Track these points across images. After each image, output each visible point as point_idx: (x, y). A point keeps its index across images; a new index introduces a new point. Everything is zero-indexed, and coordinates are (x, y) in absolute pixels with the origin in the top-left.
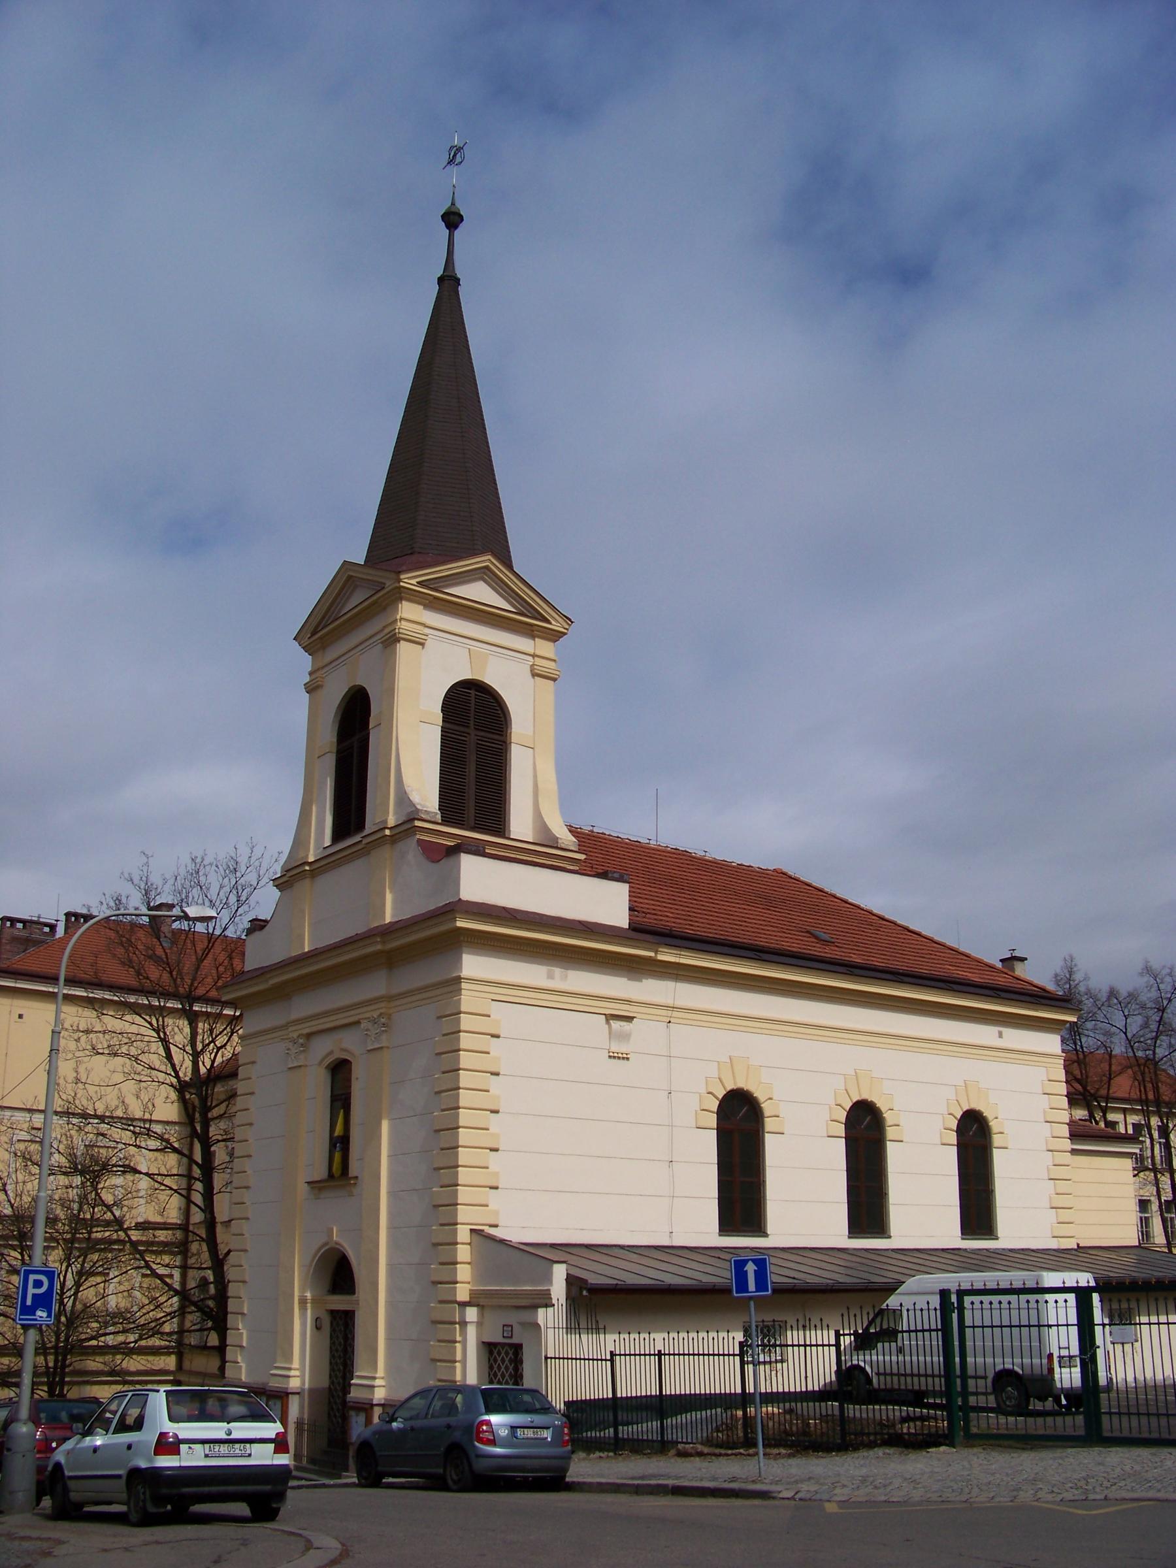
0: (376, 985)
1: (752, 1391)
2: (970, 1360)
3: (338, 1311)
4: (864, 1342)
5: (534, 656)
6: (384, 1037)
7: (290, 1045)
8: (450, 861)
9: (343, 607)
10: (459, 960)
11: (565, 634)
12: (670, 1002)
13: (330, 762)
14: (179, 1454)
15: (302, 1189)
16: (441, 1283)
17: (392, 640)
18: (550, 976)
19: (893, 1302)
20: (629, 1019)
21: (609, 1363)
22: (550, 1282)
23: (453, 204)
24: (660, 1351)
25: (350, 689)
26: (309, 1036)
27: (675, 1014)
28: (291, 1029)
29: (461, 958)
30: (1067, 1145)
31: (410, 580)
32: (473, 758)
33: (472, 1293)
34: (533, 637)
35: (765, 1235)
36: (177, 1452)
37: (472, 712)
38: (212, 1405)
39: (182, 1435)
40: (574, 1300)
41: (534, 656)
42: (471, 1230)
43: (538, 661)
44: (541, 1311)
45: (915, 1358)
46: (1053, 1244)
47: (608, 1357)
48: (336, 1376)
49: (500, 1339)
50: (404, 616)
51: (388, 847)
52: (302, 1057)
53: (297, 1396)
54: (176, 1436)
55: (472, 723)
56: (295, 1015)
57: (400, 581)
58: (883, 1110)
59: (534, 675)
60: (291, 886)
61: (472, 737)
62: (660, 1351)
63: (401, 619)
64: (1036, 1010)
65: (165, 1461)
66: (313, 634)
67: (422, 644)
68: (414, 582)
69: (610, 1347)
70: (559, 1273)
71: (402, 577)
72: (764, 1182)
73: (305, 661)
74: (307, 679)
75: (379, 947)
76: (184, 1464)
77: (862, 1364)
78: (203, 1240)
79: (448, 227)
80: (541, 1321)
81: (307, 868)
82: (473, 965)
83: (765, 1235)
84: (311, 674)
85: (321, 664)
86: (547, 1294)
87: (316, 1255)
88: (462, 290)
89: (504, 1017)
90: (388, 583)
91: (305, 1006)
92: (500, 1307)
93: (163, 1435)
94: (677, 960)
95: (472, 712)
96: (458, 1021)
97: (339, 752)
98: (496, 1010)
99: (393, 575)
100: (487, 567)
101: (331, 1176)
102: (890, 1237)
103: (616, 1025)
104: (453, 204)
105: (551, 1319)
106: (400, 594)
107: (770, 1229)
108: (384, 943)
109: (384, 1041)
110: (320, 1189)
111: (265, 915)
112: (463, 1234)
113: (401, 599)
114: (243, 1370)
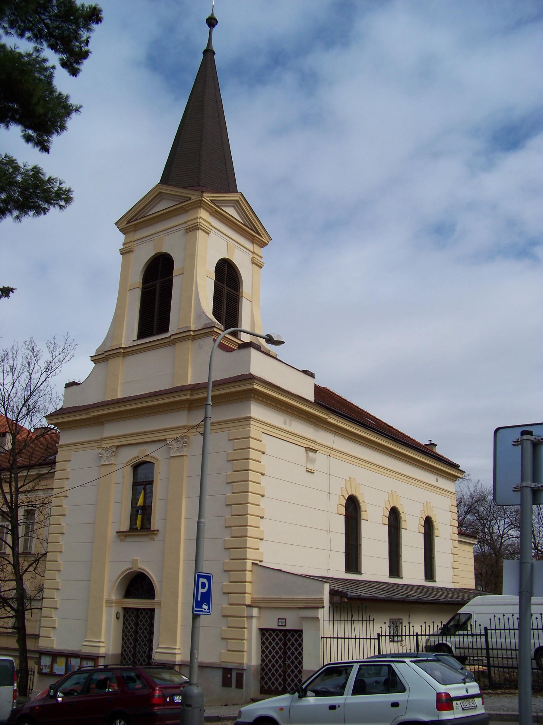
0: (181, 419)
1: (181, 655)
2: (490, 640)
3: (130, 609)
4: (446, 631)
5: (253, 253)
6: (185, 449)
7: (104, 452)
8: (243, 352)
9: (150, 210)
10: (249, 407)
11: (267, 244)
12: (331, 446)
13: (137, 294)
14: (452, 709)
15: (111, 534)
16: (231, 594)
17: (195, 228)
18: (285, 423)
19: (464, 610)
20: (315, 451)
21: (376, 641)
22: (323, 595)
23: (212, 14)
24: (417, 633)
25: (156, 254)
26: (118, 447)
27: (332, 452)
28: (103, 442)
29: (250, 406)
30: (457, 537)
31: (207, 197)
32: (225, 301)
33: (253, 600)
34: (253, 243)
35: (360, 573)
36: (450, 707)
37: (226, 276)
38: (373, 670)
39: (453, 694)
40: (334, 606)
41: (253, 253)
42: (252, 563)
43: (255, 256)
44: (320, 611)
45: (503, 640)
46: (452, 586)
47: (376, 637)
48: (128, 647)
49: (276, 627)
50: (202, 216)
51: (190, 341)
52: (113, 458)
53: (103, 659)
54: (447, 694)
55: (225, 281)
56: (105, 435)
57: (202, 196)
58: (401, 512)
59: (253, 263)
60: (107, 360)
61: (226, 290)
62: (417, 633)
63: (200, 218)
64: (451, 470)
65: (447, 715)
66: (129, 222)
67: (208, 234)
68: (208, 199)
69: (377, 631)
70: (327, 587)
71: (204, 195)
72: (360, 545)
73: (120, 238)
74: (122, 247)
75: (188, 397)
76: (457, 716)
77: (449, 644)
78: (10, 563)
79: (209, 27)
80: (320, 616)
81: (122, 351)
82: (257, 411)
83: (360, 573)
84: (124, 244)
85: (129, 240)
86: (322, 600)
87: (119, 577)
88: (215, 57)
89: (269, 443)
90: (193, 197)
91: (111, 430)
92: (275, 608)
93: (439, 695)
94: (336, 423)
95: (226, 276)
96: (249, 442)
97: (143, 288)
98: (264, 438)
99: (199, 193)
100: (237, 201)
101: (133, 528)
102: (402, 578)
103: (311, 454)
104: (212, 14)
105: (324, 614)
106: (200, 204)
107: (363, 570)
108: (191, 395)
109: (185, 452)
110: (126, 536)
111: (81, 378)
112: (249, 566)
113: (200, 207)
114: (55, 642)
